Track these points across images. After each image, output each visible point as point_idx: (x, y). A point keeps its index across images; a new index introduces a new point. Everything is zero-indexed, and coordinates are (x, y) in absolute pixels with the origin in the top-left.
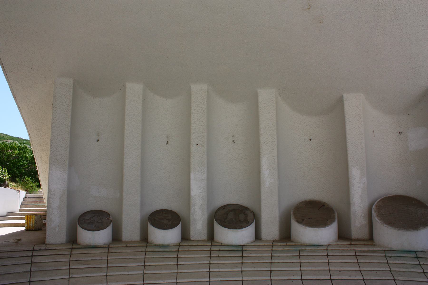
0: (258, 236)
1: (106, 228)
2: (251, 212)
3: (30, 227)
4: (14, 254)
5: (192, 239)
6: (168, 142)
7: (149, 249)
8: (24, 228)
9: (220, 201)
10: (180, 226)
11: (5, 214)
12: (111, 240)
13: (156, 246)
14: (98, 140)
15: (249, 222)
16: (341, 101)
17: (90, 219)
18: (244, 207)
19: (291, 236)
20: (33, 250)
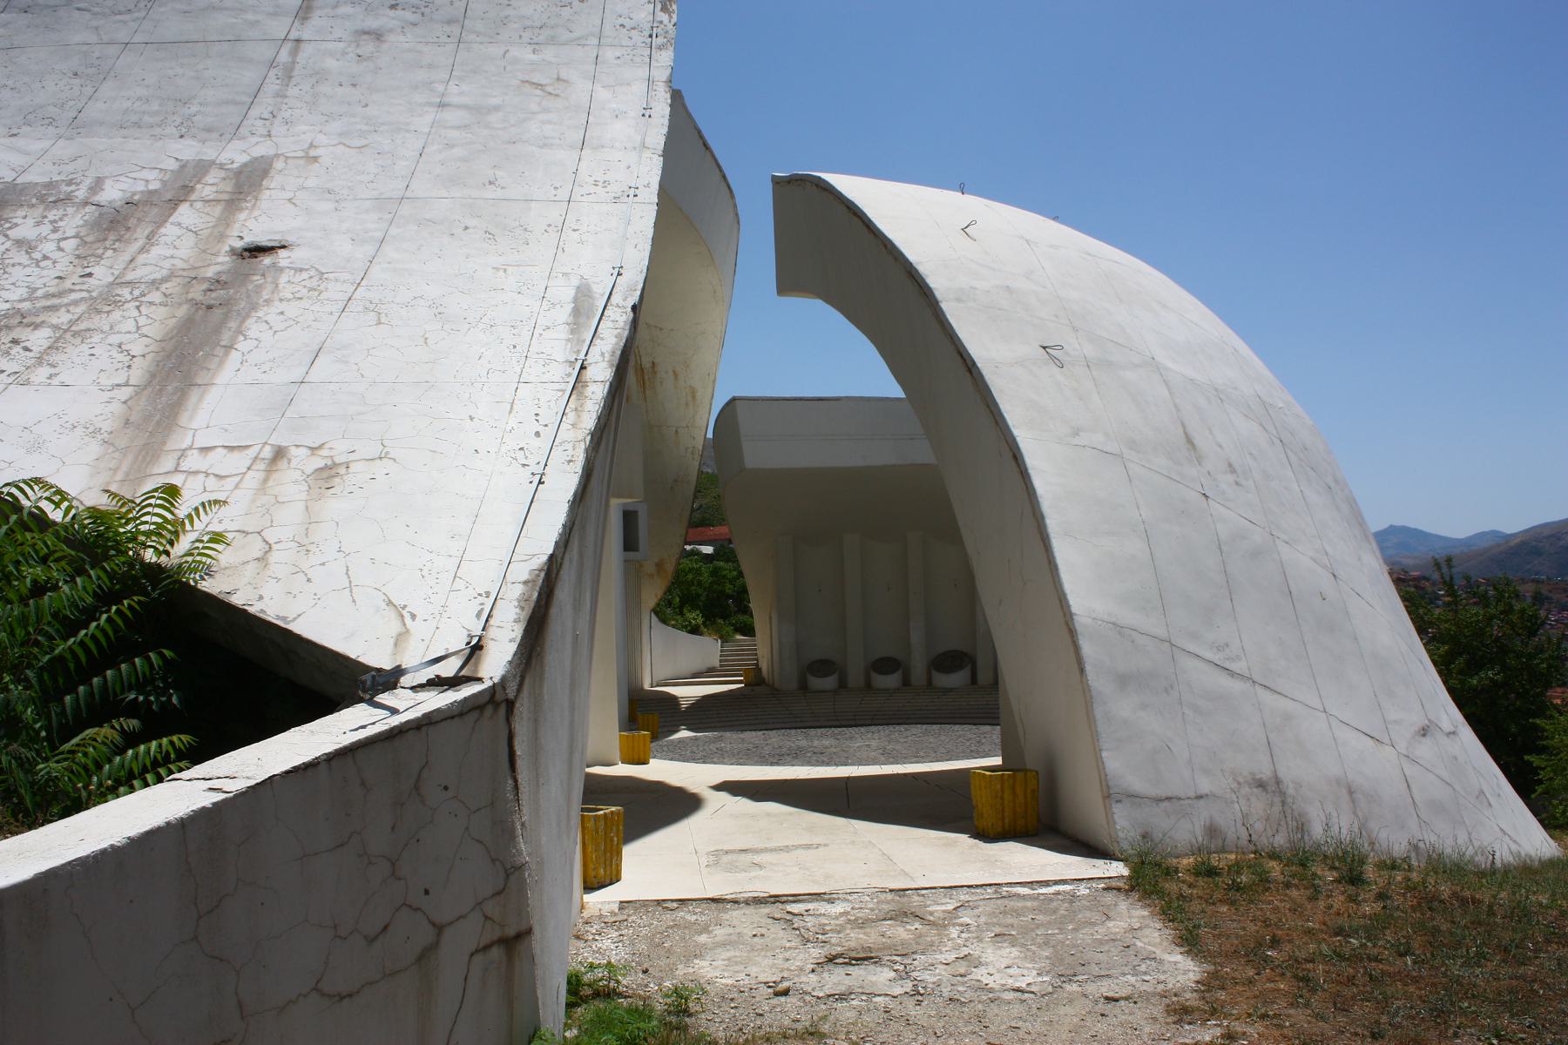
10: (900, 671)
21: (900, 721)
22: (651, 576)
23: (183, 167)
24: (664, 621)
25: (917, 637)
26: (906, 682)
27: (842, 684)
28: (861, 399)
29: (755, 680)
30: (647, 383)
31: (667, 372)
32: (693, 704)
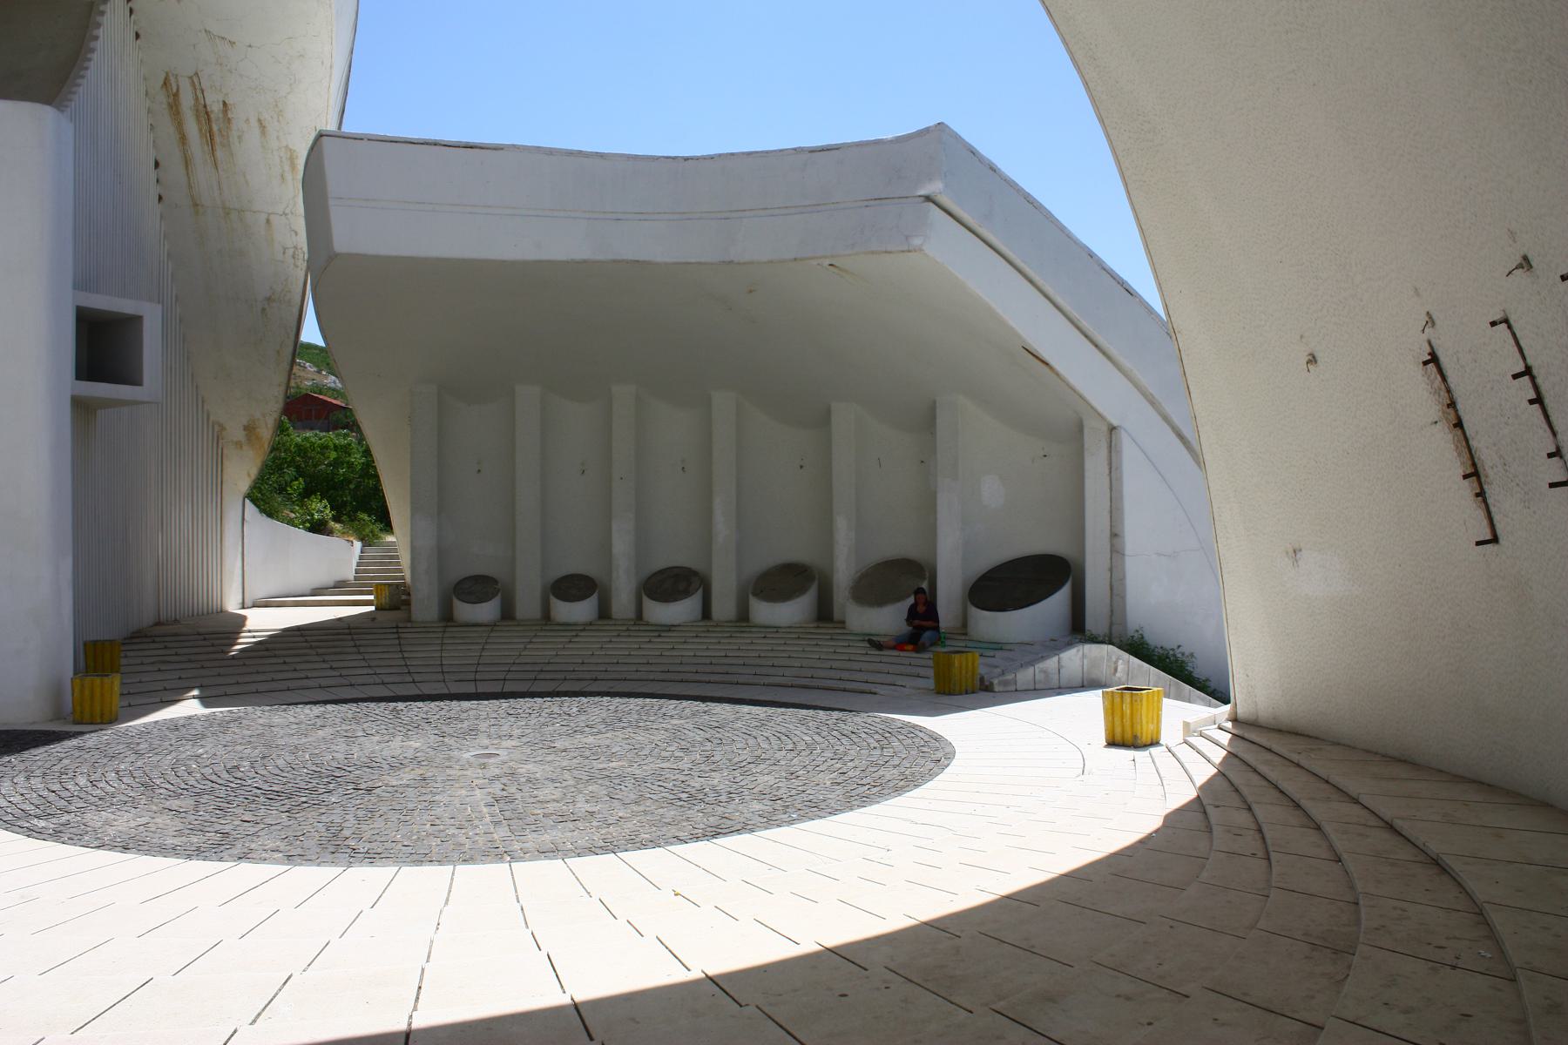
0: (706, 613)
3: (381, 604)
4: (375, 631)
5: (614, 617)
8: (372, 608)
9: (877, 554)
10: (595, 596)
11: (332, 584)
13: (559, 624)
16: (828, 413)
20: (397, 627)
21: (577, 687)
22: (239, 445)
23: (283, 262)
24: (271, 514)
25: (622, 545)
26: (604, 613)
27: (507, 614)
28: (538, 150)
29: (396, 600)
30: (217, 139)
31: (247, 120)
32: (260, 642)
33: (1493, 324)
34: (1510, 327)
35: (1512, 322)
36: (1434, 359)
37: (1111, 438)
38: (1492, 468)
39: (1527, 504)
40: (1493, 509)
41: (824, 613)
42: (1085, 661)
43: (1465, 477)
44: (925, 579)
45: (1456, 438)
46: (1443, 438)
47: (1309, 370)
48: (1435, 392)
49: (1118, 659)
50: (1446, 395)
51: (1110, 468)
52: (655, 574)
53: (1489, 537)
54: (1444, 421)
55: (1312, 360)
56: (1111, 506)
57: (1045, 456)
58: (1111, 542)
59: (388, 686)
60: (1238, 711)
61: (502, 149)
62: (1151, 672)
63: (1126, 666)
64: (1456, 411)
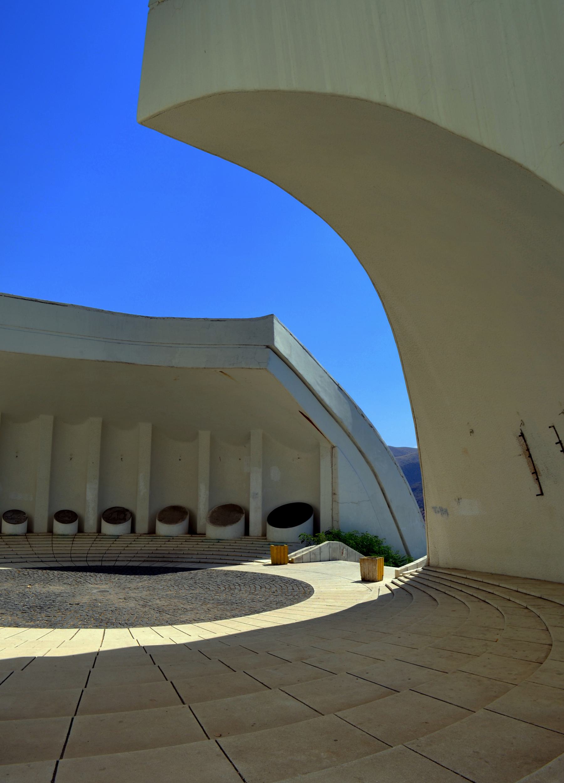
0: (133, 530)
1: (23, 523)
2: (130, 513)
6: (71, 458)
7: (54, 536)
10: (77, 522)
12: (26, 531)
14: (17, 456)
15: (126, 520)
17: (11, 516)
18: (126, 509)
19: (156, 531)
33: (550, 427)
34: (554, 428)
35: (555, 427)
36: (522, 435)
37: (332, 451)
38: (542, 471)
39: (556, 483)
40: (541, 484)
41: (192, 530)
42: (331, 549)
43: (533, 473)
44: (243, 513)
45: (528, 461)
46: (523, 461)
47: (471, 435)
48: (521, 445)
49: (344, 548)
50: (526, 446)
51: (332, 465)
52: (107, 510)
53: (539, 493)
54: (524, 455)
55: (472, 432)
56: (332, 481)
57: (299, 458)
58: (332, 496)
59: (59, 562)
60: (430, 562)
61: (67, 306)
62: (357, 554)
63: (347, 552)
64: (529, 452)
